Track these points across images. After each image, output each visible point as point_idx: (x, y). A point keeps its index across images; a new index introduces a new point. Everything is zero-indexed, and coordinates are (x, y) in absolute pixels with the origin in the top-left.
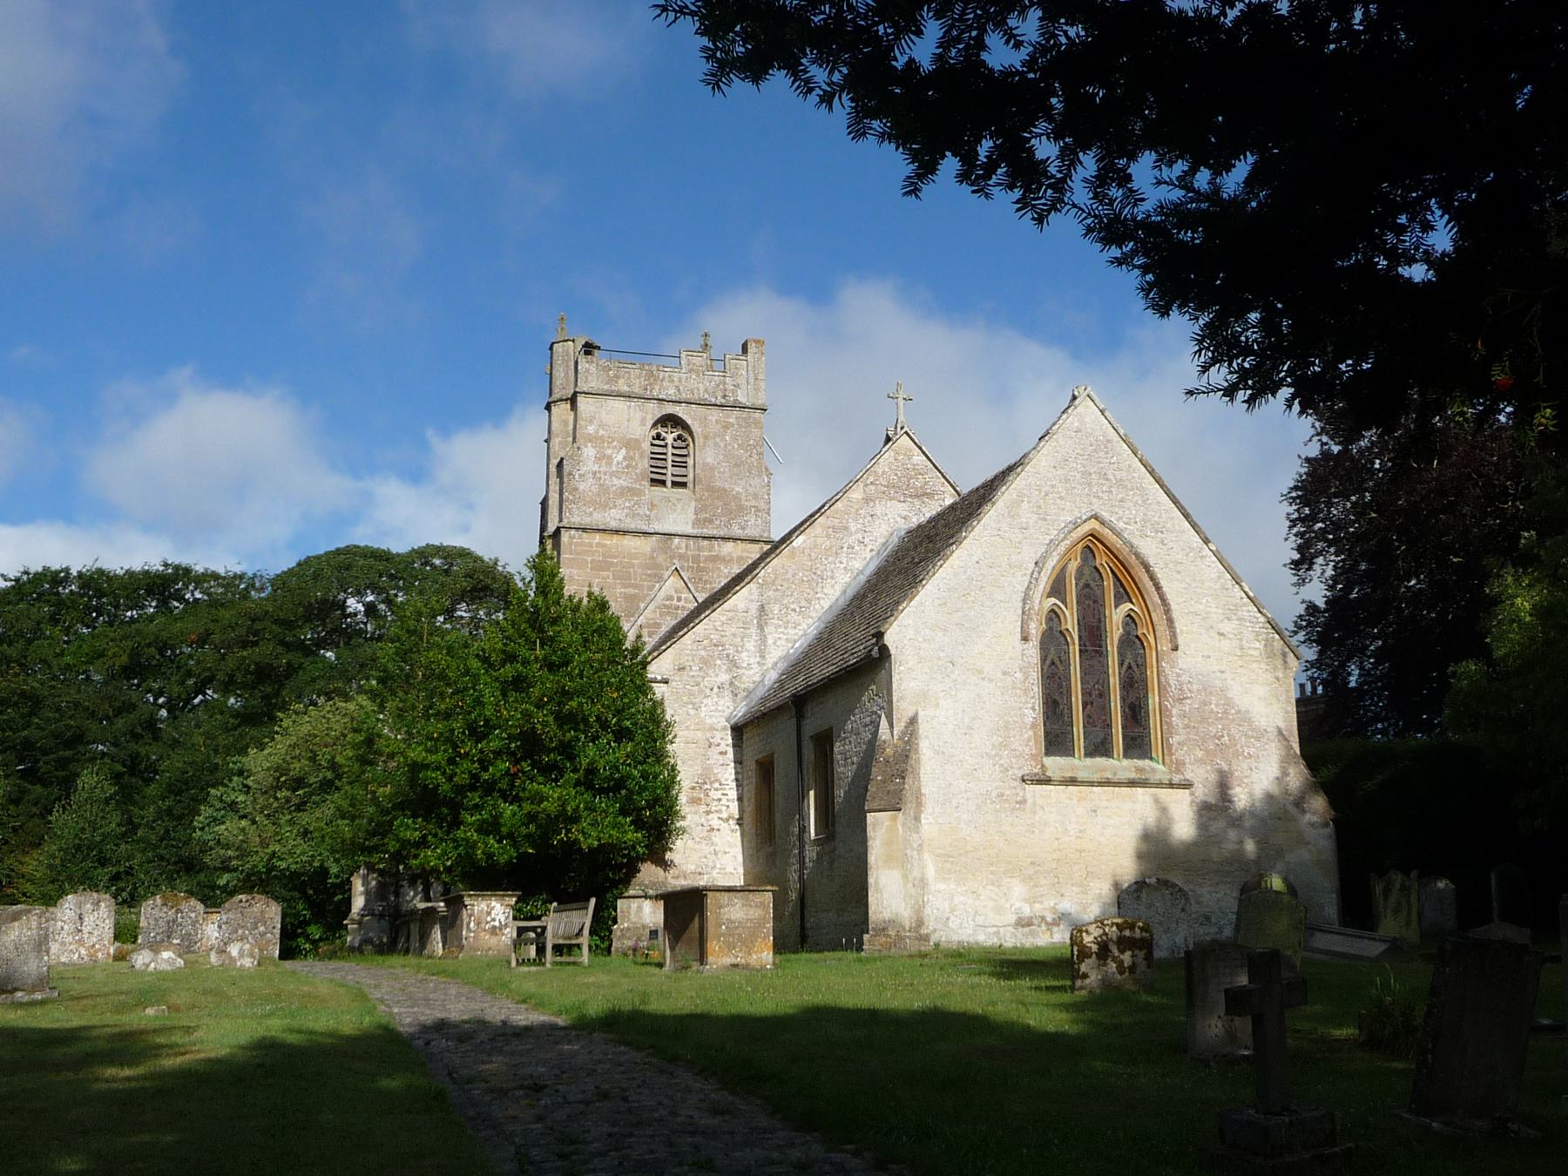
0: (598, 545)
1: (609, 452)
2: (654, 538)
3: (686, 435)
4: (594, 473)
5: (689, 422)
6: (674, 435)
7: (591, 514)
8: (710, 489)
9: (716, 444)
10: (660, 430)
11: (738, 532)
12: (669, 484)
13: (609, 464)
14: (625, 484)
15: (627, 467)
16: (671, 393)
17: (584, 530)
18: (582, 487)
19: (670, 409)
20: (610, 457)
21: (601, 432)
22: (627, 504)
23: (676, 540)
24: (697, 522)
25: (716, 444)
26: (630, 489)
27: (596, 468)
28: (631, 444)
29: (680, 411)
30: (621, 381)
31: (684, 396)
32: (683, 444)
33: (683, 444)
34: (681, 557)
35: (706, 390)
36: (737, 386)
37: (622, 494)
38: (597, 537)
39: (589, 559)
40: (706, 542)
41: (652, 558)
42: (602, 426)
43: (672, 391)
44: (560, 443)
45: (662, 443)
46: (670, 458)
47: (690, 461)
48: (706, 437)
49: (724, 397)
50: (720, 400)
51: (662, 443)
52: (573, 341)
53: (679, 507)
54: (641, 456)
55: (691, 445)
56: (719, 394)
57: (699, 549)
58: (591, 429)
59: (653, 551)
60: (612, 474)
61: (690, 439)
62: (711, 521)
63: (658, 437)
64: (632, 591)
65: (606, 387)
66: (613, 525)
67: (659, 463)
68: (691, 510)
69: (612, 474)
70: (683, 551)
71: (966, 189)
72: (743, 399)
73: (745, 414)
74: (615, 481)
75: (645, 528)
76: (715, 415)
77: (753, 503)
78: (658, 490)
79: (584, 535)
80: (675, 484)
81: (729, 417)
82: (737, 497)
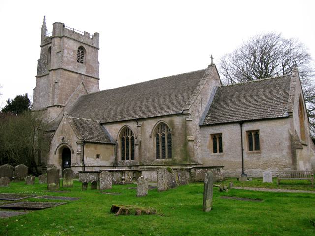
8: (88, 65)
11: (93, 76)
14: (73, 60)
16: (82, 41)
18: (64, 59)
19: (82, 45)
20: (70, 54)
24: (86, 72)
28: (74, 51)
29: (84, 46)
38: (67, 72)
42: (69, 45)
48: (88, 53)
60: (71, 58)
64: (74, 86)
66: (70, 70)
68: (85, 69)
71: (78, 24)
76: (90, 48)
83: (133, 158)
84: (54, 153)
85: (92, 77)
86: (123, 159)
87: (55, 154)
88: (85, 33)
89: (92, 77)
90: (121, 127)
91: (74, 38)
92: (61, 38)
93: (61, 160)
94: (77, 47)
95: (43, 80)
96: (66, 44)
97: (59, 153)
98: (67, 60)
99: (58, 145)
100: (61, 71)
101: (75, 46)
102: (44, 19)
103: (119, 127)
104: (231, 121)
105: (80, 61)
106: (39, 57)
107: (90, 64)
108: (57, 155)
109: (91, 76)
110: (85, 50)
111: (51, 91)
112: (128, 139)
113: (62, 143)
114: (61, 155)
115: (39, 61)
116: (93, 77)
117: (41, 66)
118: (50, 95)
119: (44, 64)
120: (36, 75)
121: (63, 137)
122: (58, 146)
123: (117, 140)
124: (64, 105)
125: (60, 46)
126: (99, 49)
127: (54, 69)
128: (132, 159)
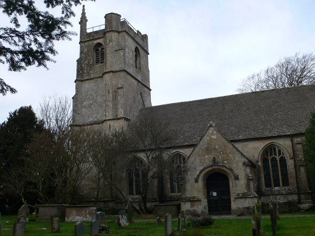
83: (286, 183)
84: (193, 181)
86: (268, 185)
87: (196, 181)
88: (138, 31)
90: (263, 146)
92: (119, 32)
93: (206, 190)
95: (86, 85)
97: (204, 180)
99: (201, 168)
100: (123, 74)
102: (84, 10)
103: (261, 145)
106: (78, 57)
108: (200, 184)
110: (139, 52)
111: (111, 99)
112: (274, 160)
113: (212, 166)
114: (205, 182)
115: (79, 62)
117: (81, 67)
118: (111, 105)
119: (88, 65)
120: (75, 78)
122: (202, 171)
123: (258, 162)
124: (129, 118)
125: (118, 42)
127: (113, 70)
128: (284, 185)
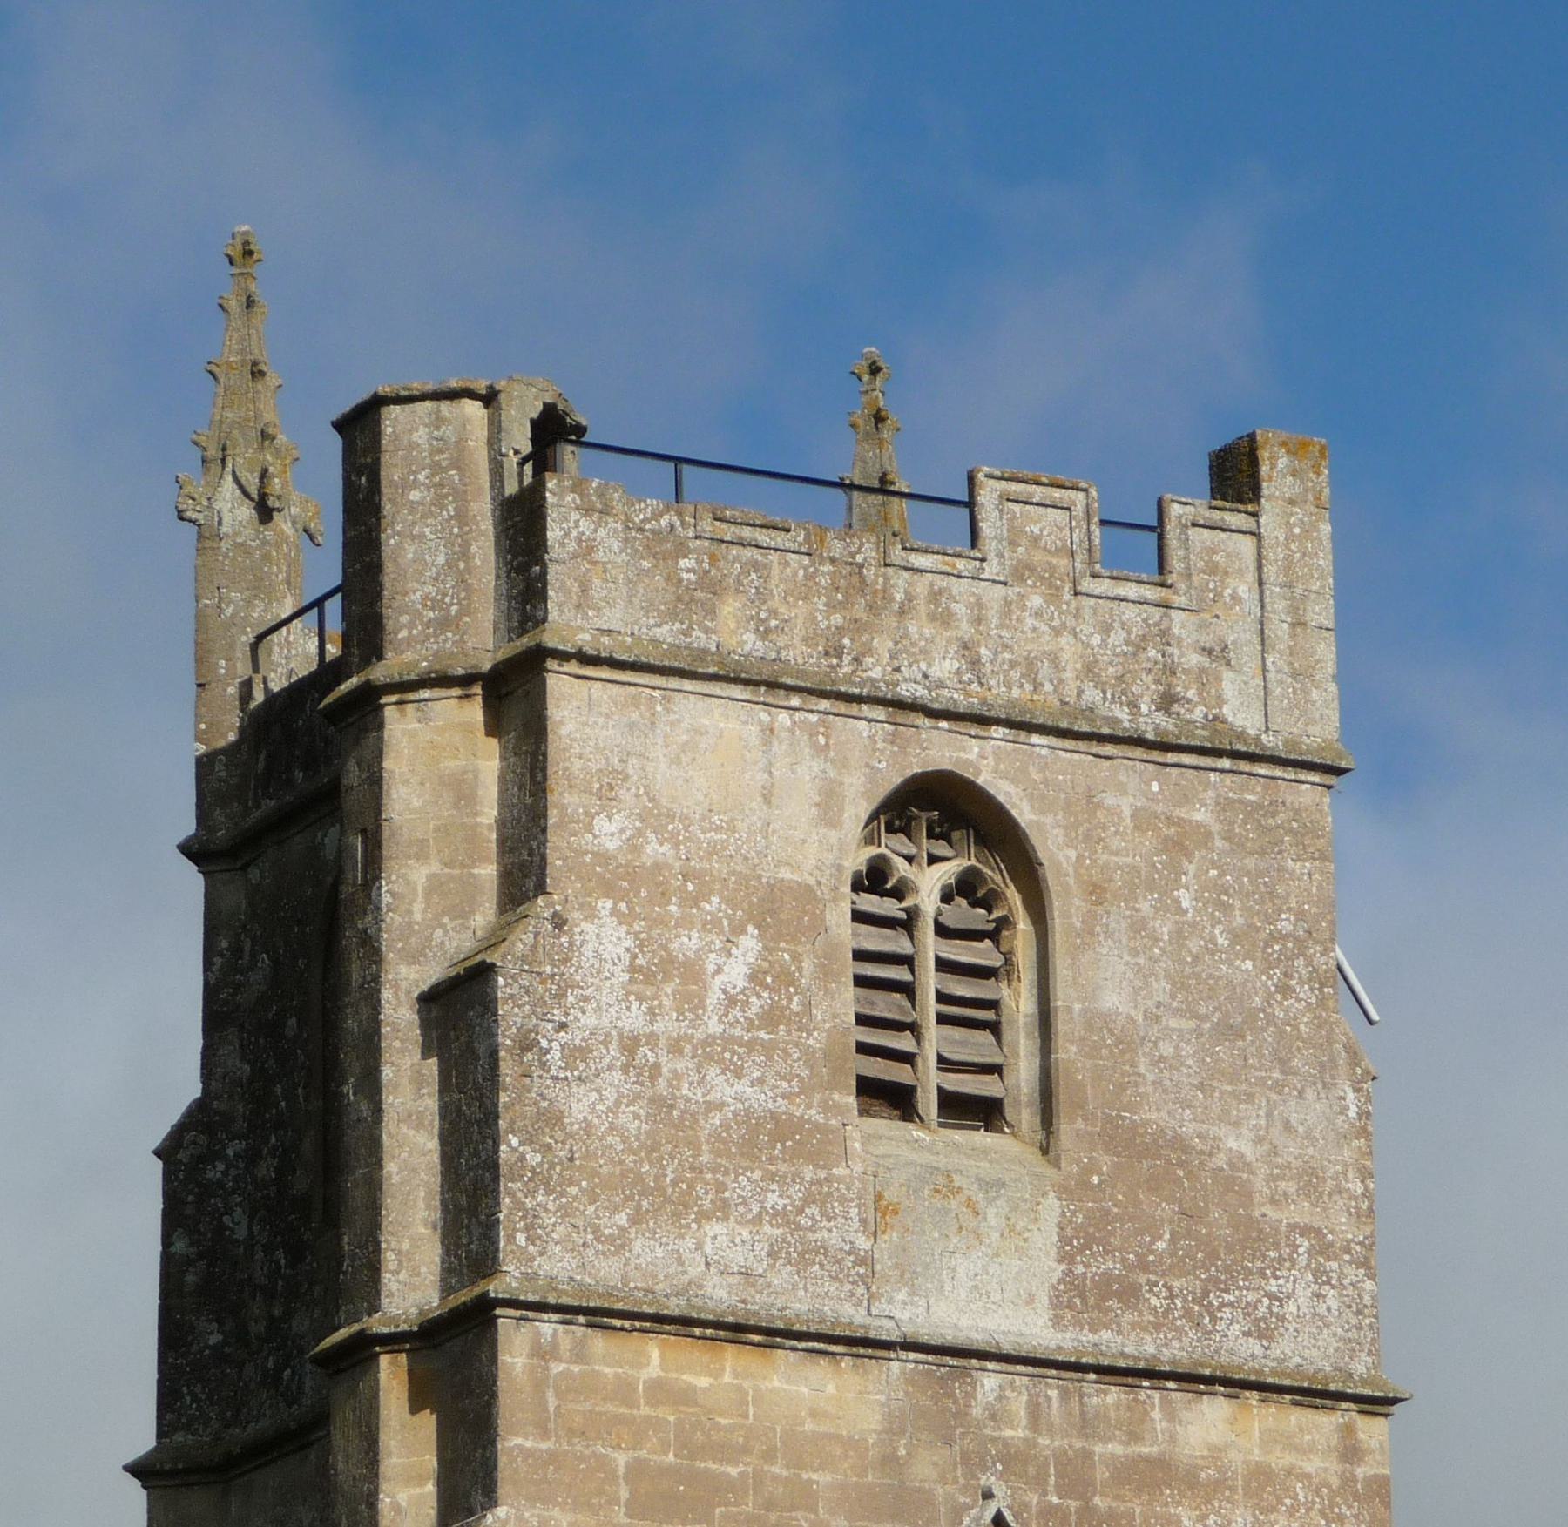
0: (660, 1391)
1: (688, 943)
2: (897, 1367)
3: (996, 876)
4: (630, 1045)
5: (1023, 813)
6: (946, 872)
7: (619, 1242)
9: (1139, 926)
10: (892, 846)
12: (928, 1103)
13: (692, 1002)
15: (771, 1018)
17: (598, 1316)
18: (580, 1106)
20: (692, 973)
21: (655, 849)
22: (773, 1199)
23: (990, 1381)
25: (1139, 926)
26: (782, 1128)
27: (634, 1019)
30: (730, 608)
31: (1004, 692)
32: (978, 918)
33: (978, 918)
34: (1014, 1461)
35: (1090, 670)
36: (1219, 653)
37: (749, 1149)
39: (621, 1459)
40: (1113, 1396)
41: (889, 1461)
42: (654, 817)
43: (945, 667)
44: (435, 886)
45: (888, 907)
46: (930, 981)
47: (1019, 1002)
48: (1096, 892)
49: (1167, 701)
50: (1151, 722)
51: (888, 907)
52: (490, 399)
53: (994, 1216)
54: (826, 973)
55: (1023, 924)
56: (1146, 690)
57: (1087, 1425)
58: (609, 832)
59: (894, 1427)
60: (708, 1052)
61: (1014, 897)
62: (1129, 1294)
63: (874, 879)
65: (666, 633)
66: (720, 1296)
67: (887, 1005)
68: (1044, 1239)
69: (708, 1052)
70: (1016, 1433)
72: (1243, 716)
73: (1254, 787)
74: (723, 1088)
75: (853, 1316)
77: (1300, 1212)
78: (886, 1127)
79: (599, 1342)
80: (959, 1109)
81: (1185, 799)
82: (1233, 1184)
85: (1192, 1380)
89: (1192, 1380)
91: (748, 645)
94: (828, 806)
96: (607, 797)
98: (632, 1121)
101: (798, 810)
104: (1262, 1415)
105: (930, 1082)
107: (1155, 1115)
109: (1173, 1351)
116: (1235, 1385)
121: (283, 524)
126: (140, 1470)
